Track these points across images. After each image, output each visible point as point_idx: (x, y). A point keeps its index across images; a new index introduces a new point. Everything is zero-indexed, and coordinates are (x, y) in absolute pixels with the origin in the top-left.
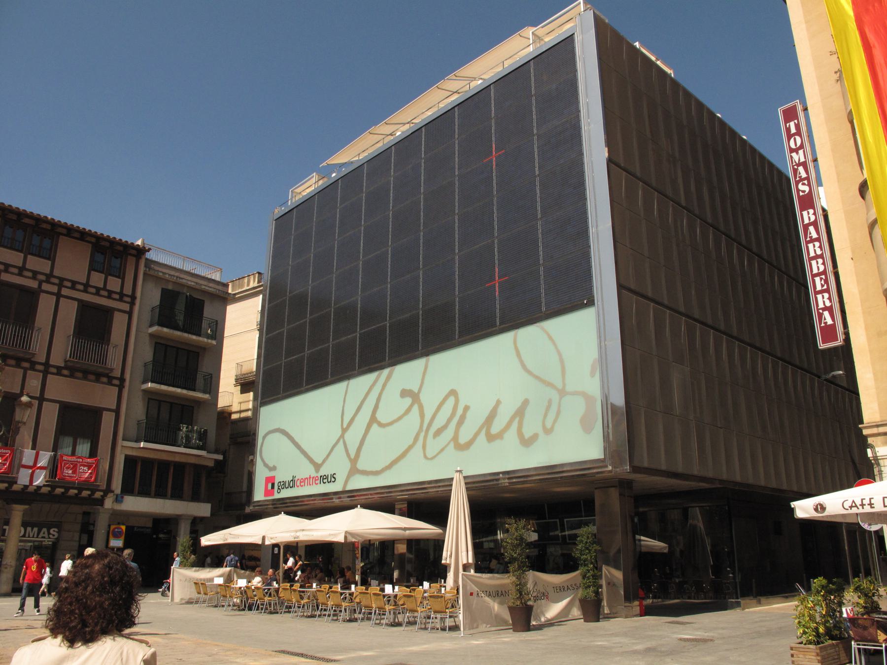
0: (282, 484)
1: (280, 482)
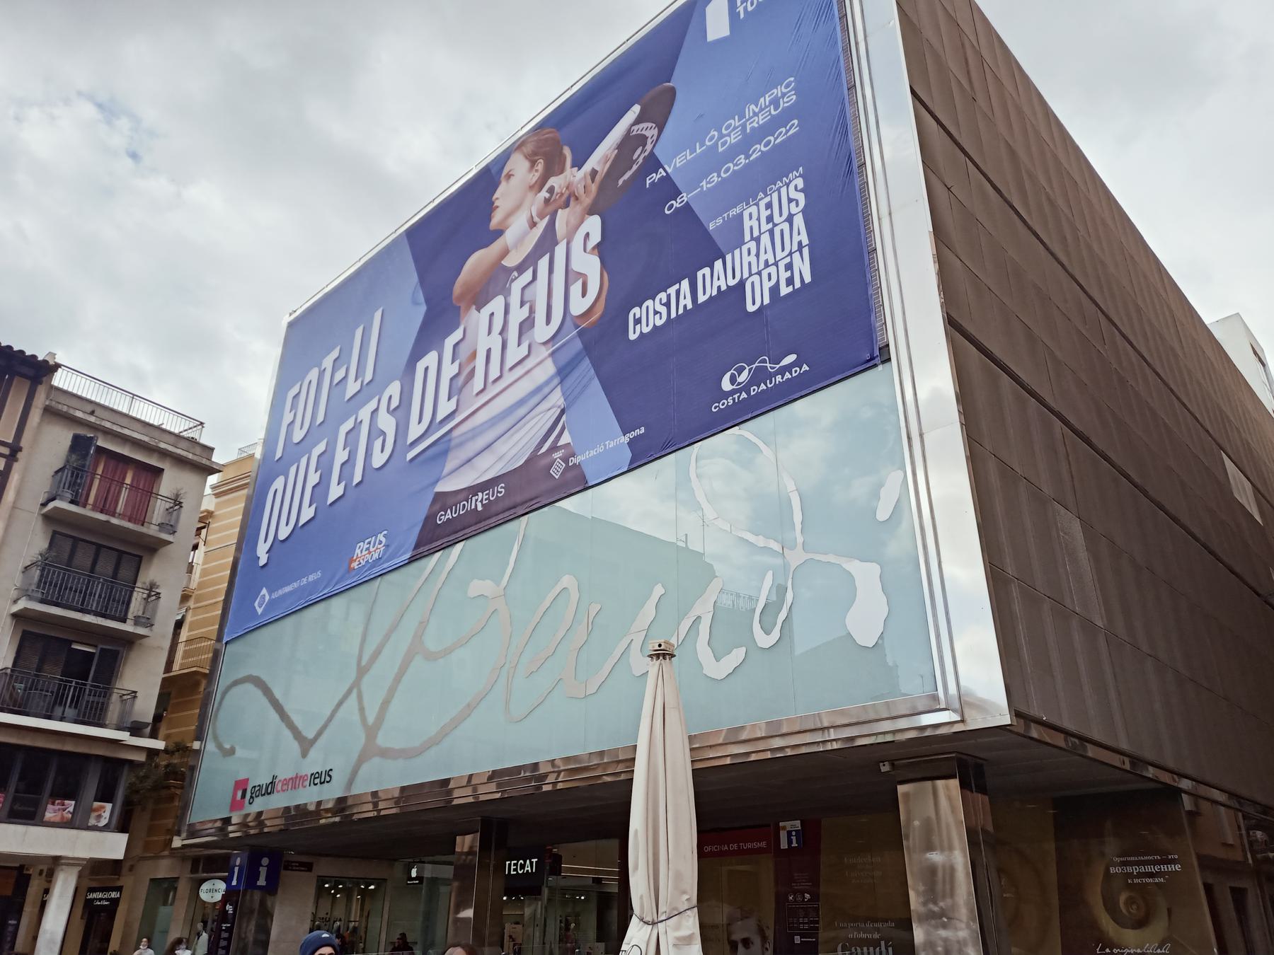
0: (257, 789)
1: (255, 787)
